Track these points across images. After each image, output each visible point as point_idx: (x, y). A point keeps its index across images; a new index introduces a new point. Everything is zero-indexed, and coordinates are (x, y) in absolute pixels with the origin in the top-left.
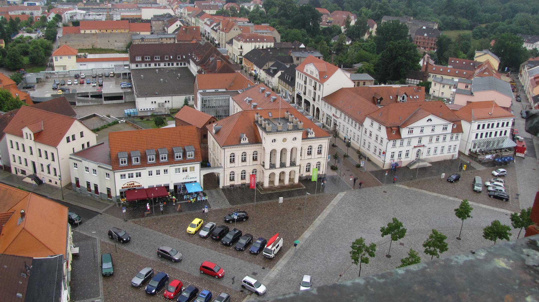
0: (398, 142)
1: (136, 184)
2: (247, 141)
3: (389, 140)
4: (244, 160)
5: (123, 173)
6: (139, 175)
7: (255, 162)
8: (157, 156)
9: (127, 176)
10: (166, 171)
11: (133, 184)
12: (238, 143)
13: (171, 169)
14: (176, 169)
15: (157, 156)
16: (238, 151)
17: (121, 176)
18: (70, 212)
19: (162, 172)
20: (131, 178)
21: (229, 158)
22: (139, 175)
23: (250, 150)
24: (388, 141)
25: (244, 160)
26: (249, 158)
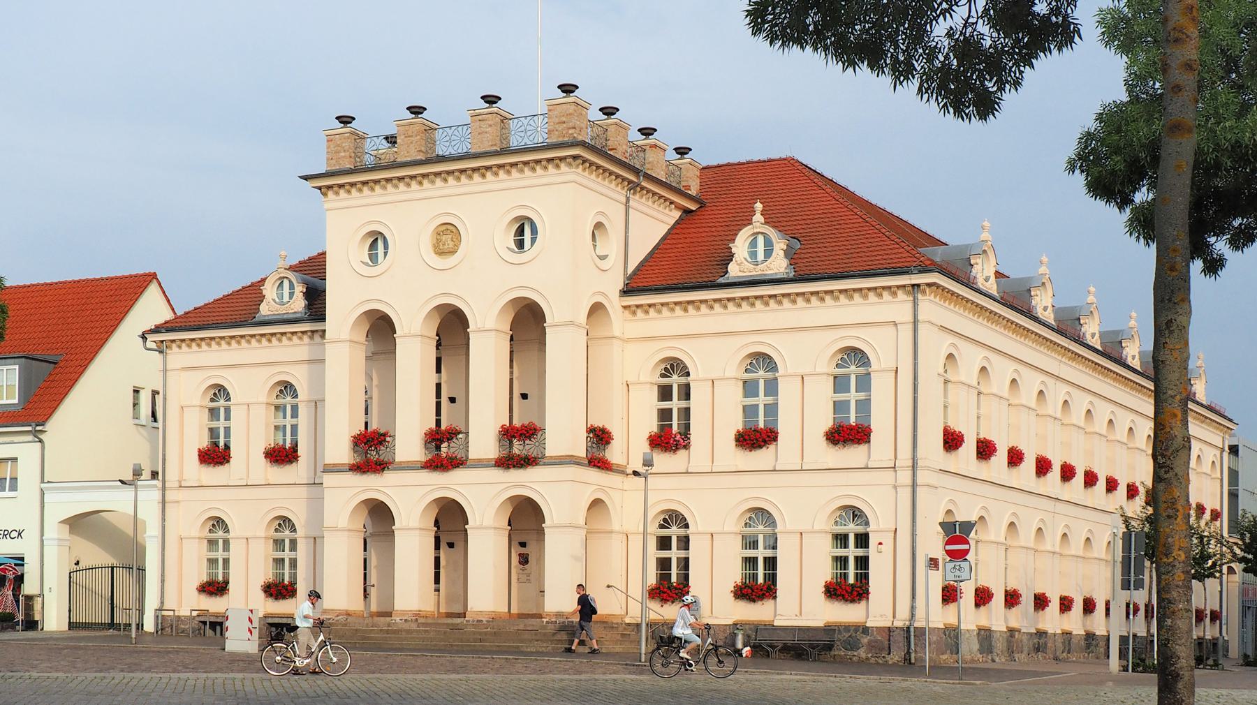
2: (778, 265)
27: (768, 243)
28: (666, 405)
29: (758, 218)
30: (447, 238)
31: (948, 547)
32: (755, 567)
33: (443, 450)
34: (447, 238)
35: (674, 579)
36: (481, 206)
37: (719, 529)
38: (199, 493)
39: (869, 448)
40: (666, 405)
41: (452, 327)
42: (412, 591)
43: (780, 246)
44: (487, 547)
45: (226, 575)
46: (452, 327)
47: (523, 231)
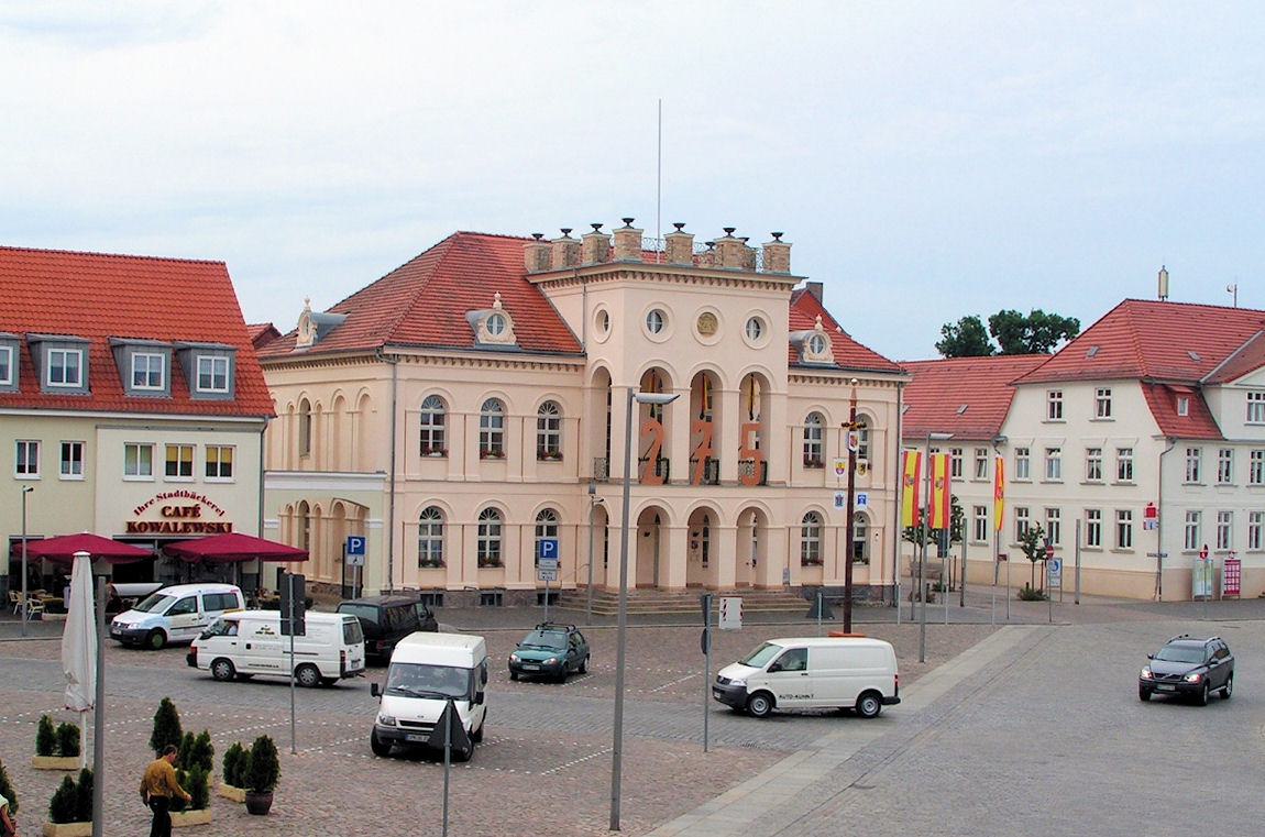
0: (1210, 457)
1: (207, 516)
2: (506, 337)
3: (1171, 440)
4: (492, 448)
5: (140, 437)
6: (220, 468)
7: (551, 470)
8: (180, 372)
9: (160, 460)
10: (72, 453)
11: (195, 511)
12: (461, 343)
13: (108, 445)
14: (130, 448)
15: (180, 372)
16: (465, 390)
17: (130, 448)
18: (63, 603)
19: (50, 456)
20: (179, 478)
21: (415, 428)
22: (220, 468)
23: (524, 390)
24: (1163, 445)
25: (492, 448)
26: (521, 438)
27: (500, 322)
28: (553, 432)
29: (497, 304)
30: (708, 323)
31: (1228, 658)
32: (426, 547)
33: (707, 470)
34: (708, 323)
35: (488, 555)
36: (684, 302)
37: (469, 522)
38: (423, 481)
39: (447, 466)
40: (553, 432)
41: (705, 385)
42: (676, 570)
43: (509, 324)
44: (725, 544)
45: (1017, 588)
46: (705, 385)
47: (658, 319)
